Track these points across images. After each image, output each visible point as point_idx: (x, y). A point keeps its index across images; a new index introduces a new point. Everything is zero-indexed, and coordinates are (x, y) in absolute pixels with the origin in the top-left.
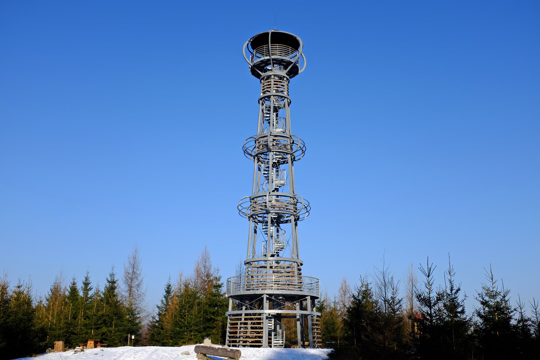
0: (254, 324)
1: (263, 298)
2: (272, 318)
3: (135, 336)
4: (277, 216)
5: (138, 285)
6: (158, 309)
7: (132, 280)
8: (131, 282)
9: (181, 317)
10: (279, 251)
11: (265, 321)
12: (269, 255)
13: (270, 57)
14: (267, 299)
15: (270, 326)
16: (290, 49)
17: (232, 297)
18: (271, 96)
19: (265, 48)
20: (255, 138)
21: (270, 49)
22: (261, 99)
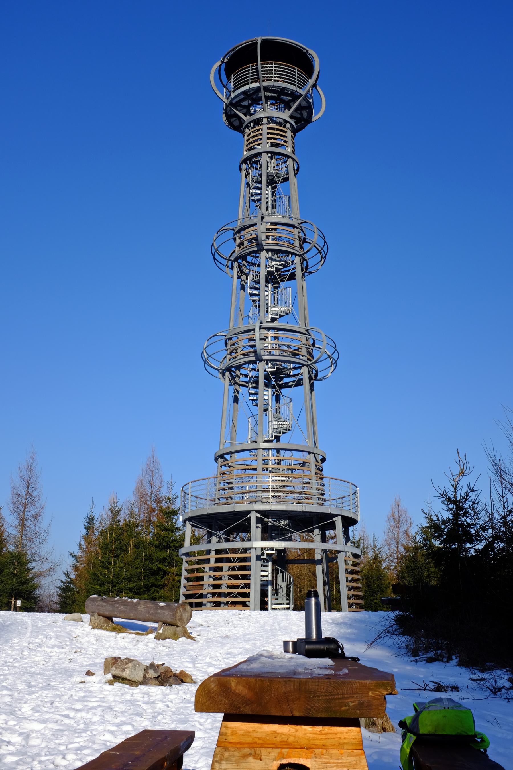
0: (233, 569)
2: (268, 561)
3: (22, 602)
4: (275, 370)
5: (36, 516)
6: (73, 559)
7: (25, 506)
8: (24, 510)
9: (103, 567)
10: (280, 433)
11: (254, 564)
12: (260, 439)
13: (260, 84)
14: (259, 521)
15: (264, 576)
16: (296, 71)
18: (263, 154)
19: (250, 68)
21: (260, 69)
22: (245, 161)
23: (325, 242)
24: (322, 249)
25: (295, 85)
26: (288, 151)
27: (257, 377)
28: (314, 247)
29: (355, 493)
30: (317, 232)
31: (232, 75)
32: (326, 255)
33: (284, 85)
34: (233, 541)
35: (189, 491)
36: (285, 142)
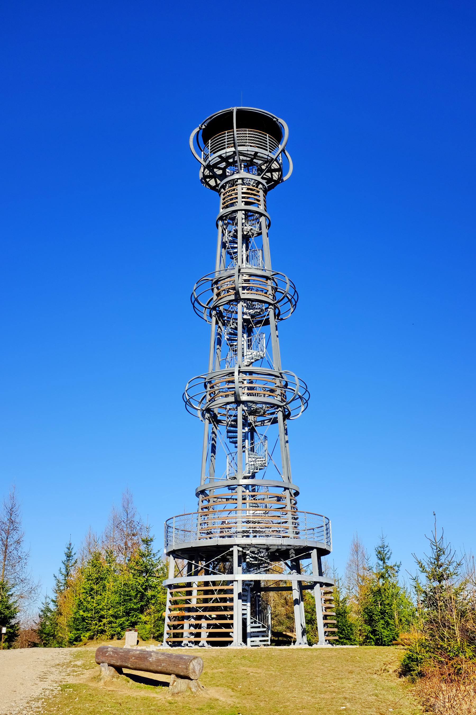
1: (231, 554)
5: (18, 542)
12: (239, 476)
13: (235, 149)
20: (205, 378)
22: (221, 218)
23: (295, 291)
24: (292, 297)
25: (267, 150)
26: (261, 209)
27: (236, 416)
31: (210, 141)
32: (296, 303)
33: (257, 150)
35: (173, 525)
36: (259, 201)
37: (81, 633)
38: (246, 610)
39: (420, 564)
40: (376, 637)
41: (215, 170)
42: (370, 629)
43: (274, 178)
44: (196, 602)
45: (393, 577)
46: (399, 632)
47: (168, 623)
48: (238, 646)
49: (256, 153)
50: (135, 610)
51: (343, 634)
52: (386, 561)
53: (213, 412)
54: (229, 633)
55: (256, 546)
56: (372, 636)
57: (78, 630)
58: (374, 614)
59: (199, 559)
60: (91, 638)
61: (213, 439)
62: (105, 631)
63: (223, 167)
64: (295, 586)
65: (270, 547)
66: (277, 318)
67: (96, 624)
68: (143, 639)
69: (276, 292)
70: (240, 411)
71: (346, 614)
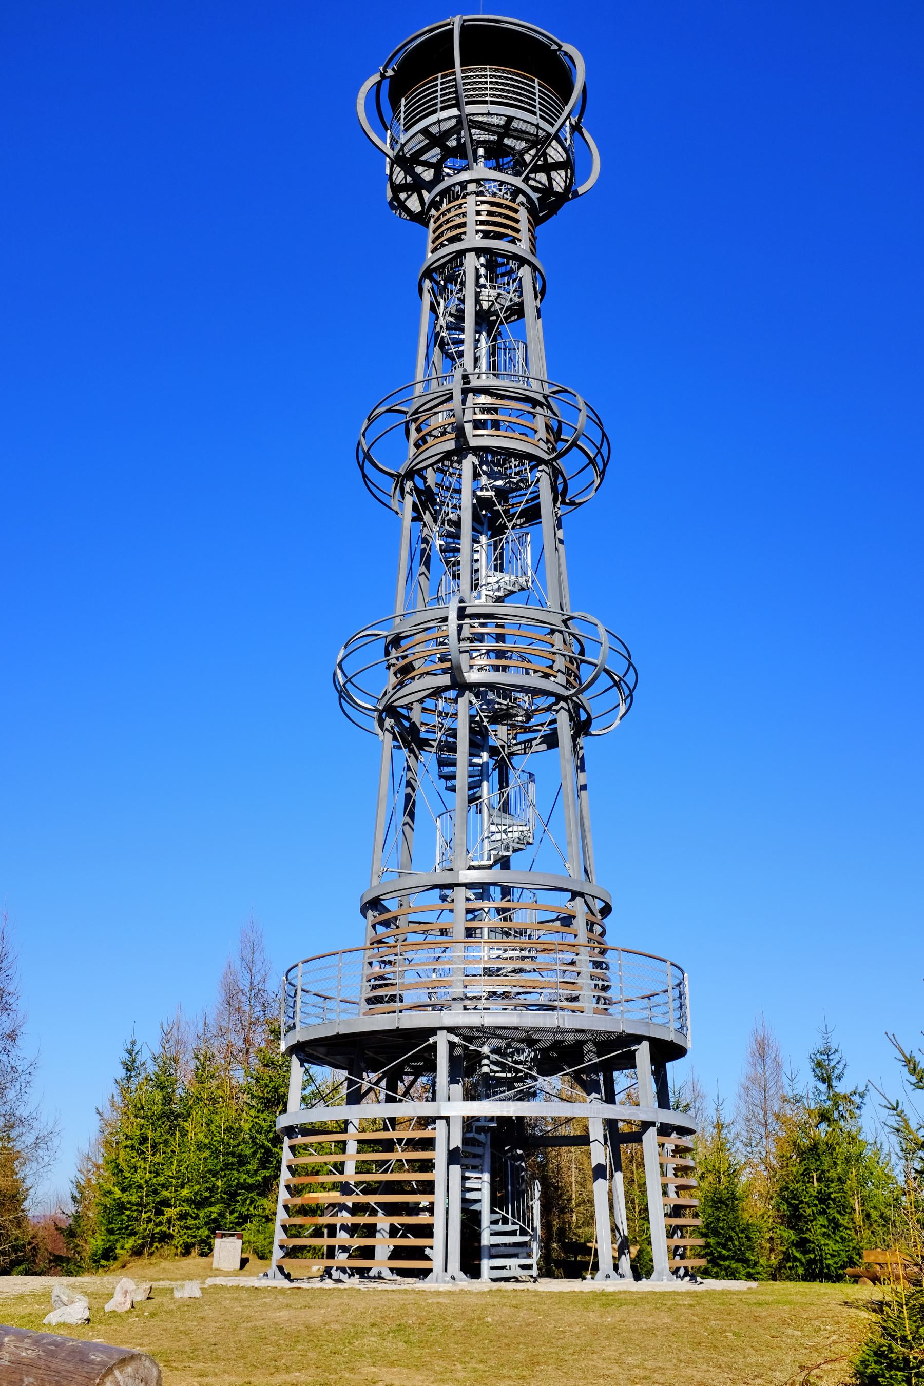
12: (460, 863)
13: (459, 110)
17: (299, 1049)
22: (428, 273)
25: (534, 113)
26: (523, 248)
28: (603, 674)
29: (678, 985)
30: (584, 411)
31: (403, 100)
32: (605, 465)
34: (401, 1101)
37: (117, 1241)
38: (479, 1190)
39: (912, 1066)
40: (807, 1256)
41: (419, 169)
42: (793, 1237)
43: (557, 188)
44: (354, 1171)
45: (849, 1119)
46: (861, 1244)
47: (282, 1220)
48: (445, 1282)
49: (510, 119)
50: (249, 1188)
51: (729, 1250)
52: (834, 1083)
53: (408, 719)
54: (422, 1249)
55: (498, 1032)
56: (798, 1255)
57: (111, 1232)
58: (802, 1202)
59: (363, 1065)
60: (137, 1252)
61: (409, 784)
62: (171, 1237)
63: (434, 160)
64: (597, 1132)
65: (534, 1037)
66: (560, 499)
67: (149, 1220)
68: (258, 1254)
69: (559, 443)
70: (465, 706)
71: (736, 1202)
